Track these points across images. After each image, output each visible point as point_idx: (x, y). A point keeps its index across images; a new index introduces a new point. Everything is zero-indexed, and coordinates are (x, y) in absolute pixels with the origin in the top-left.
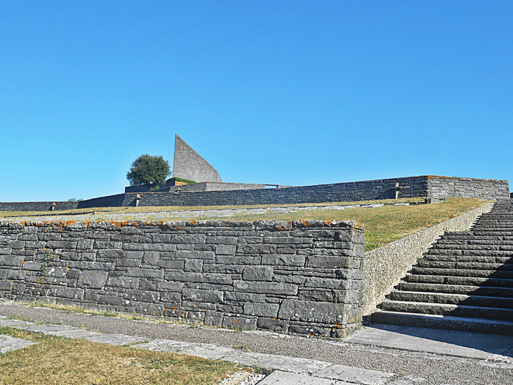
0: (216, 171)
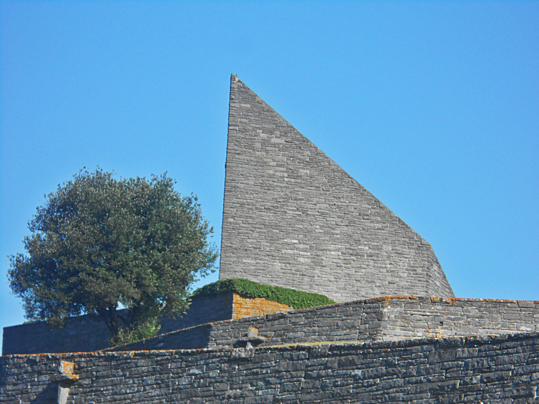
0: (422, 247)
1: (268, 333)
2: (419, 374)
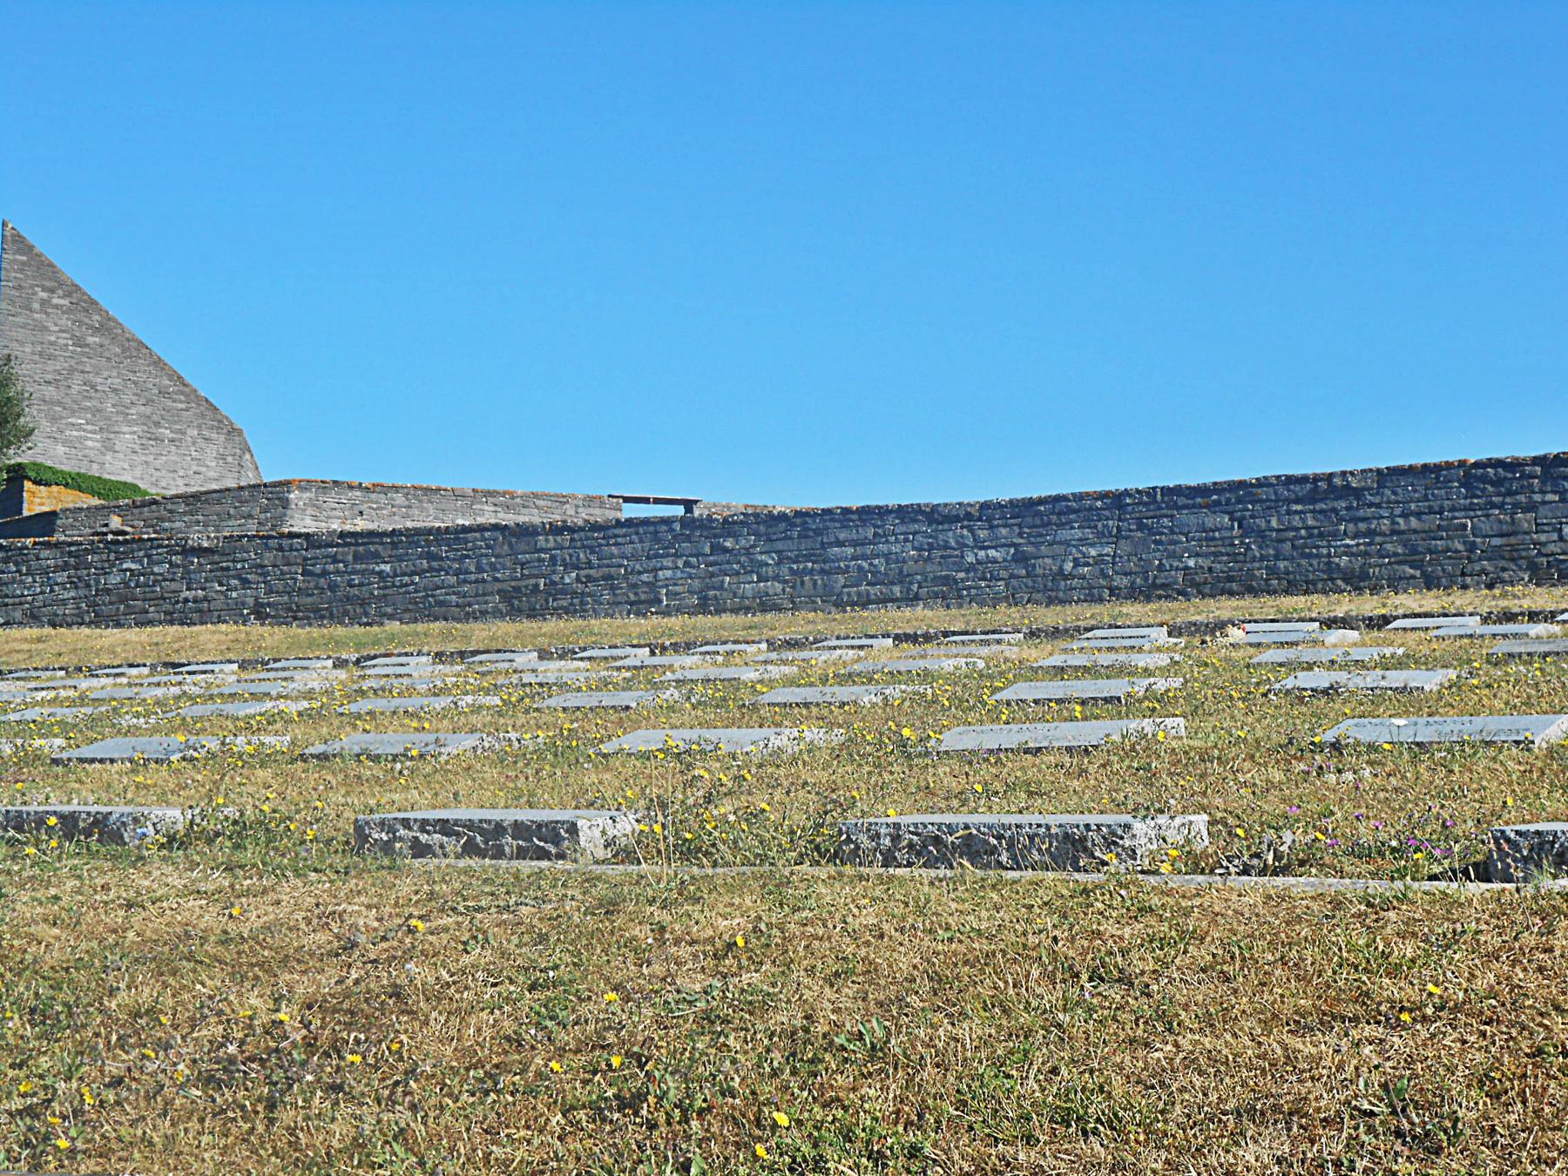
0: (233, 432)
1: (136, 523)
2: (480, 570)
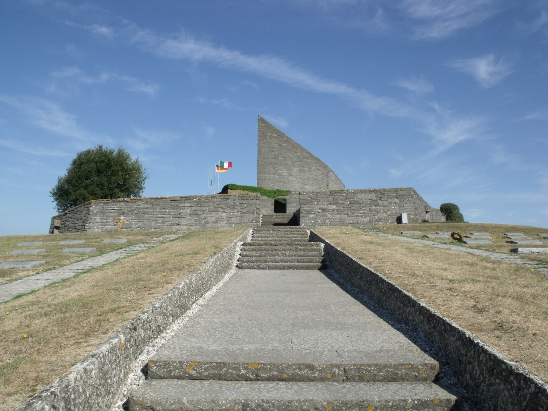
0: (325, 167)
